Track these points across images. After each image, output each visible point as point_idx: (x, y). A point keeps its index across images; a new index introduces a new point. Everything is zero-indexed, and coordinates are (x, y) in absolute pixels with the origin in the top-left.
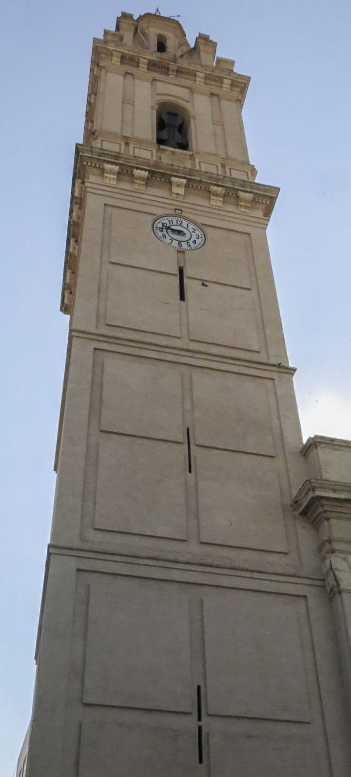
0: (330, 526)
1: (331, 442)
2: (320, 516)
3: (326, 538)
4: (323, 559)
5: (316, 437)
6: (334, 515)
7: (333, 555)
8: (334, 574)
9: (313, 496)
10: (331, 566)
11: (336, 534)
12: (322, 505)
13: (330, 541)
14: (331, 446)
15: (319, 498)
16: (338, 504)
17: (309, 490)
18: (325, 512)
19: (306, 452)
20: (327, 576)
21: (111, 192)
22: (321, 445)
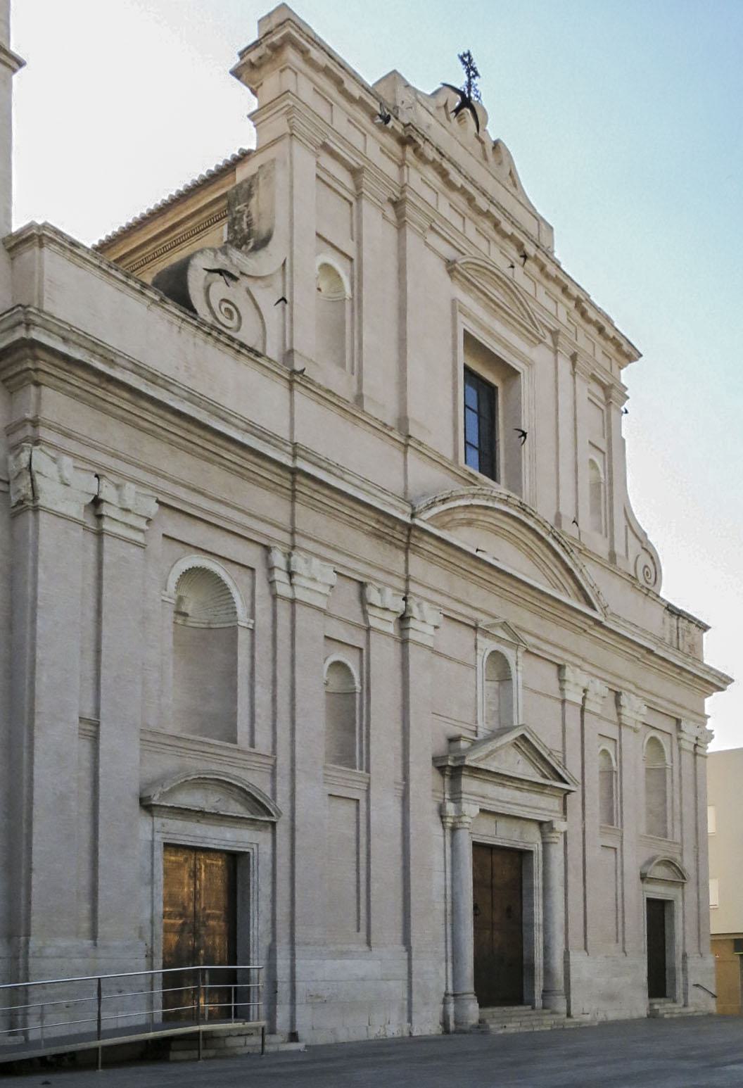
0: (39, 398)
1: (72, 248)
2: (24, 375)
3: (29, 416)
4: (15, 448)
5: (45, 226)
6: (52, 380)
7: (38, 448)
8: (32, 480)
9: (24, 336)
10: (30, 465)
11: (47, 414)
12: (36, 358)
13: (35, 423)
14: (68, 254)
15: (34, 344)
16: (63, 365)
17: (19, 323)
18: (37, 370)
19: (16, 245)
20: (16, 478)
21: (271, 116)
22: (52, 246)
